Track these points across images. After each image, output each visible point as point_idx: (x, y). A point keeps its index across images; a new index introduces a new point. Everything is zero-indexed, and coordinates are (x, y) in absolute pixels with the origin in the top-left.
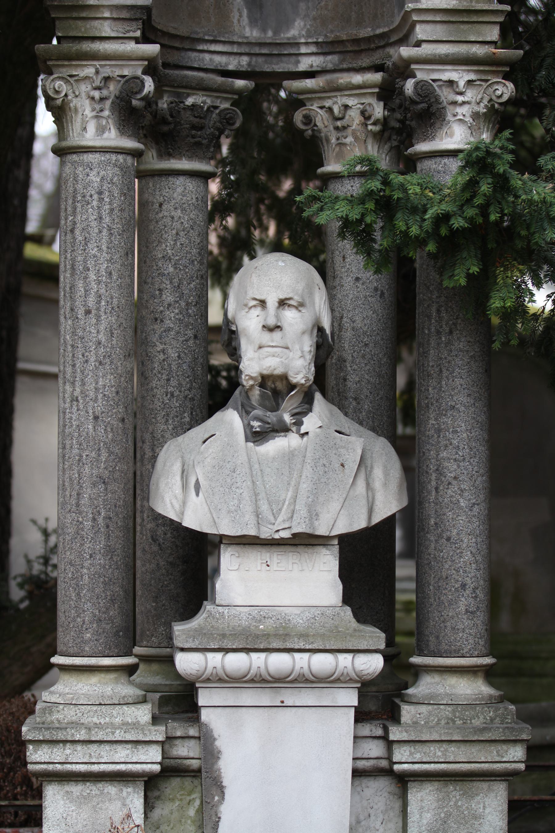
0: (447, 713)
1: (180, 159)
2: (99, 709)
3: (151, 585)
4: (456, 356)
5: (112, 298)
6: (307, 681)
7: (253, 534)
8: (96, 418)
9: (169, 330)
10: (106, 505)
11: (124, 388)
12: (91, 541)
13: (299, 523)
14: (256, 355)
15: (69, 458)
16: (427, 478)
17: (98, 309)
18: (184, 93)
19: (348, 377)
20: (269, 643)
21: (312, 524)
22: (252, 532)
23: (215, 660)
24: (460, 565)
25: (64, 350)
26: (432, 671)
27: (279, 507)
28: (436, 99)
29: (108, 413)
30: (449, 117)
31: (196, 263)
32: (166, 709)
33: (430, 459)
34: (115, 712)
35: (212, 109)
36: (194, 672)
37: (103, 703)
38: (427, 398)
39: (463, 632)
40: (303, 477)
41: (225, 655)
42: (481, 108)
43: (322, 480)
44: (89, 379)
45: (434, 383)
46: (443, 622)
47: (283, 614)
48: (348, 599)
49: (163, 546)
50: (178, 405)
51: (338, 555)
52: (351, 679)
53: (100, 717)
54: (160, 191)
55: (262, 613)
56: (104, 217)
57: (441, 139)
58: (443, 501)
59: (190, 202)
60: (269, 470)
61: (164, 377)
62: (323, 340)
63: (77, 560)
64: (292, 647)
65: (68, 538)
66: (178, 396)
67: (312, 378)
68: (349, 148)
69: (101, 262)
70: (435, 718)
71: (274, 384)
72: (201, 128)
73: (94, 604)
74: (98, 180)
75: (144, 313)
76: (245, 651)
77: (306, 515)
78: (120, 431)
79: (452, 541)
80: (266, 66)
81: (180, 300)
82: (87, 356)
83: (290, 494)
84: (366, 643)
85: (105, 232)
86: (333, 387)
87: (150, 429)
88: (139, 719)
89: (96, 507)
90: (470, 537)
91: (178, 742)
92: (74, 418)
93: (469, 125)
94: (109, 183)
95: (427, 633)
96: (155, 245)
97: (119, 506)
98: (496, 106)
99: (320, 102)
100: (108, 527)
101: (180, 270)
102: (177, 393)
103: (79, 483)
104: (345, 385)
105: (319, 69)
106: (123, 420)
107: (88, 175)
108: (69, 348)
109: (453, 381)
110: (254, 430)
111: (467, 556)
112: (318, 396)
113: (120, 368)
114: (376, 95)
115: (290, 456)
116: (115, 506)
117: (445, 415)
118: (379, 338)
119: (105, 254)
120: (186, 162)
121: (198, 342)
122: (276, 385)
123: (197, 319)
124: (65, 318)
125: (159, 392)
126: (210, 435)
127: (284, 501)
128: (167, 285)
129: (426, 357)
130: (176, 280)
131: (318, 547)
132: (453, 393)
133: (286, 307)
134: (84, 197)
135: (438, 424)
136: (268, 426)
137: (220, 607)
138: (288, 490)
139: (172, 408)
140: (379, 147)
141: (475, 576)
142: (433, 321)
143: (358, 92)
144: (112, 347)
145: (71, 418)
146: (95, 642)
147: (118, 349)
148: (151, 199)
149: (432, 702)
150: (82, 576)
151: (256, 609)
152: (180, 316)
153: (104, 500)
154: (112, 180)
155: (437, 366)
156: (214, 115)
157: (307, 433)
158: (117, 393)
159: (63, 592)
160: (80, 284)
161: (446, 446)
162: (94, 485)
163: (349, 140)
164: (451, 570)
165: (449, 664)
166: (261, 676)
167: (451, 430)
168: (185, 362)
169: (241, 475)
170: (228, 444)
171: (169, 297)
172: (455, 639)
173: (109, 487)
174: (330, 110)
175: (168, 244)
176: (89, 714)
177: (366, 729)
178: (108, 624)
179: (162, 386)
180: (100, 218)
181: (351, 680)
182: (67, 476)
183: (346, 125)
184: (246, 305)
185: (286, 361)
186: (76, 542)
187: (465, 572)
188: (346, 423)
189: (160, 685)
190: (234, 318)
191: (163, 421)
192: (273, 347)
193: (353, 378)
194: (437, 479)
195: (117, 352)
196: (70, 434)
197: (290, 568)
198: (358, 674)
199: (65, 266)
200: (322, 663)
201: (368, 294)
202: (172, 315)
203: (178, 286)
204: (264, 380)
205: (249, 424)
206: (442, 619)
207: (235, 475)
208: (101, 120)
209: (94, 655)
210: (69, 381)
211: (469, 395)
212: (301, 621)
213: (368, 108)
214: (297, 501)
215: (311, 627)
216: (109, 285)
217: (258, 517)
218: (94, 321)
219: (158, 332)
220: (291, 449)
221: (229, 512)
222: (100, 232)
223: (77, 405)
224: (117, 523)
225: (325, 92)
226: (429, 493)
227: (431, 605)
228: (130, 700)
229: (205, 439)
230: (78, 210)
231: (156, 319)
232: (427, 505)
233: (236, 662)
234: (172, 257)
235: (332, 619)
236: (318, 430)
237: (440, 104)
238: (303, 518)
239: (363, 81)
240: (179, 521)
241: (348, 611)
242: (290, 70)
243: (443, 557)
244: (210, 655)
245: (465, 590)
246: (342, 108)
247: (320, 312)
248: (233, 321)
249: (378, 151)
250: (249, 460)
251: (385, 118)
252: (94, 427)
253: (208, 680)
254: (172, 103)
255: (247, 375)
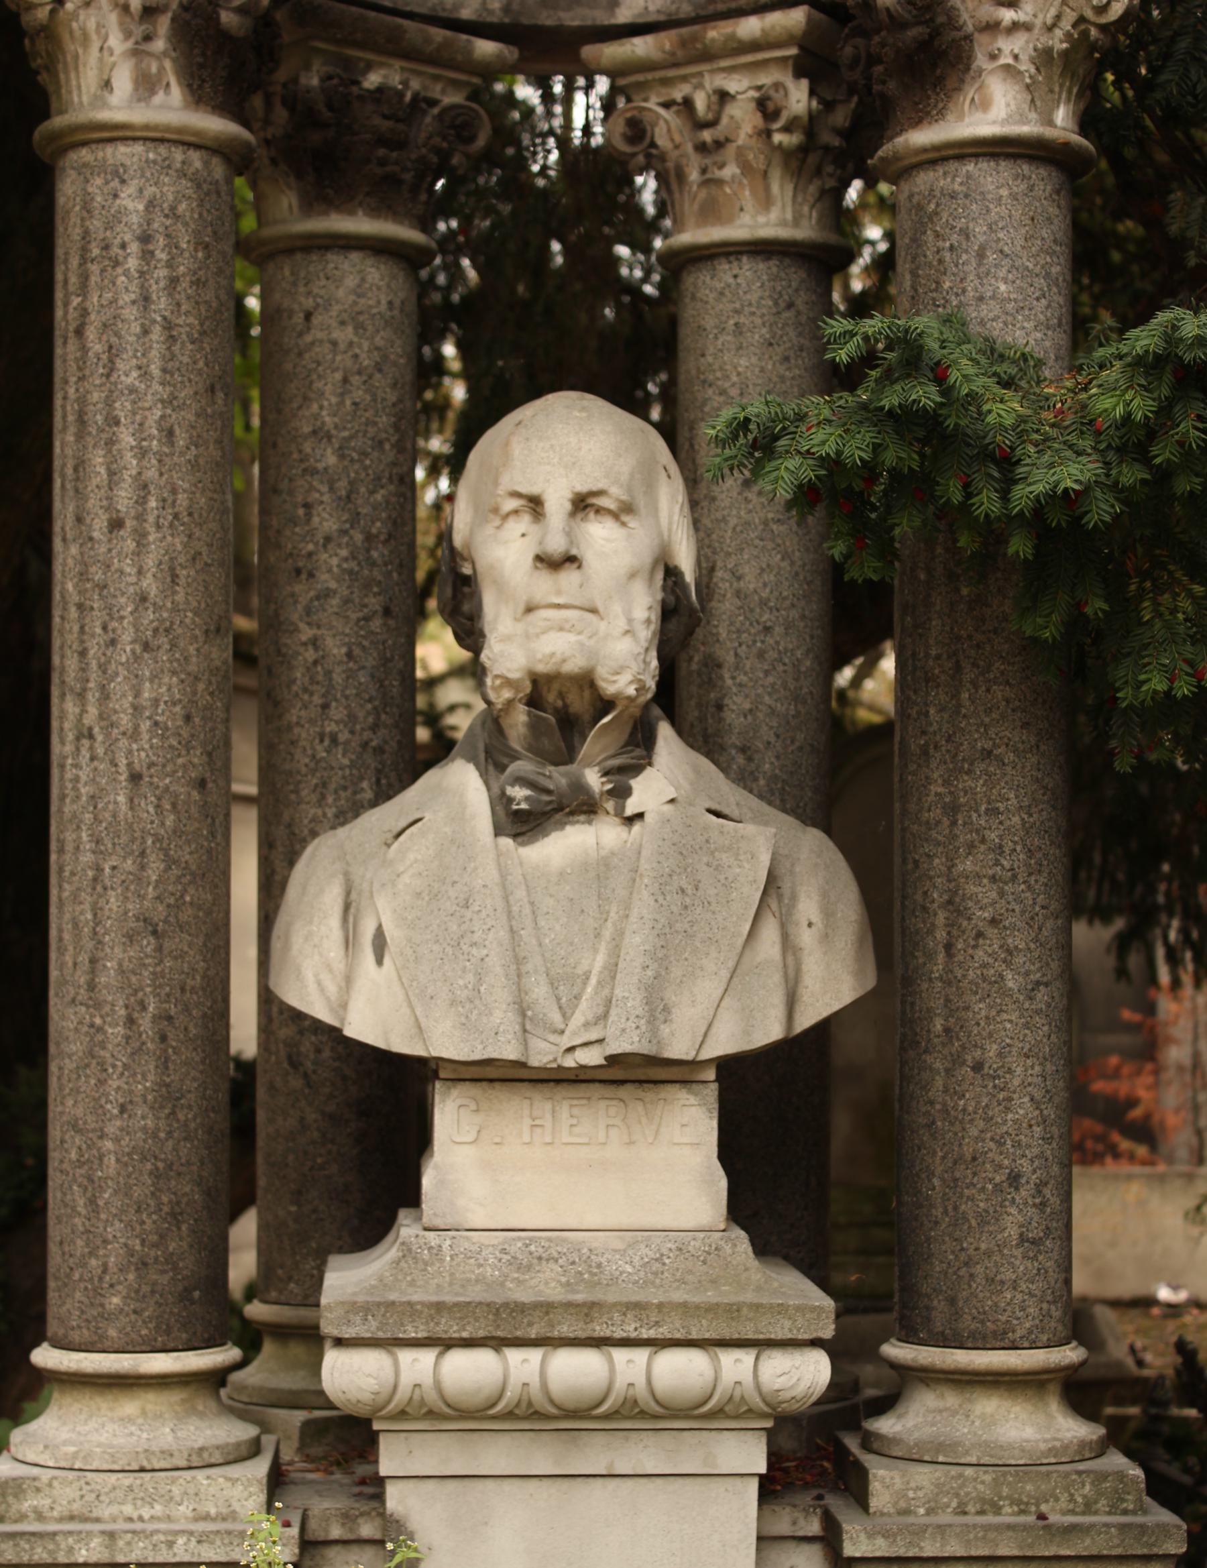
0: (981, 1487)
1: (351, 213)
2: (138, 1482)
3: (287, 1165)
4: (995, 631)
5: (174, 491)
6: (643, 1414)
7: (512, 1057)
8: (135, 778)
9: (327, 594)
10: (160, 986)
11: (205, 708)
12: (122, 1074)
13: (624, 1030)
14: (520, 628)
15: (73, 874)
16: (924, 922)
17: (140, 518)
18: (360, 59)
19: (726, 701)
20: (552, 1326)
21: (654, 1031)
22: (510, 1052)
23: (417, 1365)
24: (1005, 1128)
25: (63, 618)
26: (938, 1381)
27: (576, 991)
28: (950, 18)
29: (164, 766)
30: (981, 60)
31: (387, 446)
32: (317, 1450)
33: (931, 878)
34: (176, 1491)
35: (424, 105)
36: (366, 1397)
37: (148, 1467)
38: (924, 733)
39: (1015, 1288)
40: (634, 918)
41: (440, 1355)
42: (1057, 41)
43: (678, 926)
44: (118, 686)
45: (942, 697)
46: (966, 1264)
47: (585, 1251)
48: (740, 1210)
49: (314, 1077)
50: (346, 762)
51: (716, 1106)
52: (750, 1410)
53: (139, 1502)
54: (306, 285)
55: (532, 1248)
56: (154, 297)
57: (961, 118)
58: (964, 976)
59: (374, 311)
60: (551, 902)
61: (317, 700)
62: (678, 598)
63: (89, 1118)
64: (608, 1333)
65: (69, 1065)
66: (347, 742)
67: (652, 684)
68: (728, 190)
69: (147, 405)
70: (951, 1501)
71: (563, 699)
72: (400, 144)
73: (129, 1225)
74: (141, 207)
75: (272, 559)
76: (493, 1343)
77: (639, 1011)
78: (194, 810)
79: (986, 1070)
80: (545, 14)
81: (352, 527)
82: (114, 630)
83: (600, 960)
84: (787, 1324)
85: (157, 334)
86: (692, 726)
87: (286, 817)
88: (236, 1506)
89: (136, 991)
90: (1029, 1062)
91: (332, 1552)
92: (84, 778)
93: (1028, 81)
94: (166, 216)
95: (925, 1289)
96: (295, 405)
97: (193, 988)
98: (1094, 32)
99: (664, 91)
100: (163, 1038)
101: (352, 460)
102: (344, 736)
103: (95, 933)
104: (721, 720)
105: (662, 18)
106: (202, 784)
107: (116, 196)
108: (73, 613)
109: (988, 690)
110: (515, 807)
111: (1023, 1109)
112: (665, 732)
113: (194, 659)
114: (790, 62)
115: (600, 870)
116: (183, 990)
117: (968, 772)
118: (794, 614)
119: (156, 387)
120: (365, 219)
121: (392, 622)
122: (568, 701)
123: (390, 573)
124: (64, 540)
125: (304, 734)
126: (411, 819)
127: (587, 976)
128: (322, 494)
129: (921, 635)
130: (342, 486)
131: (669, 1087)
132: (987, 720)
133: (592, 515)
134: (106, 247)
135: (951, 793)
136: (546, 798)
137: (432, 1234)
138: (596, 951)
139: (332, 768)
140: (795, 188)
141: (1041, 1156)
142: (939, 550)
143: (749, 58)
144: (175, 609)
145: (77, 779)
146: (133, 1317)
147: (189, 614)
148: (286, 303)
149: (941, 1459)
150: (101, 1158)
151: (519, 1239)
152: (352, 565)
153: (154, 973)
154: (173, 209)
155: (949, 657)
156: (428, 120)
157: (640, 816)
158: (188, 718)
159: (59, 1195)
160: (98, 459)
161: (971, 846)
162: (130, 938)
163: (730, 171)
164: (983, 1140)
165: (983, 1367)
166: (530, 1404)
167: (983, 808)
168: (363, 668)
169: (483, 914)
170: (453, 841)
171: (327, 521)
172: (996, 1305)
173: (168, 945)
174: (688, 103)
175: (326, 403)
176: (112, 1495)
177: (783, 1523)
178: (163, 1272)
179: (312, 721)
180: (145, 299)
181: (751, 1413)
182: (67, 916)
183: (722, 139)
184: (495, 510)
185: (592, 642)
186: (87, 1076)
187: (1017, 1144)
188: (731, 795)
189: (306, 1391)
190: (468, 545)
191: (314, 798)
192: (558, 606)
193: (737, 704)
194: (950, 924)
195: (187, 621)
196: (74, 816)
197: (601, 1136)
198: (768, 1399)
199: (64, 417)
200: (681, 1371)
201: (770, 515)
202: (335, 561)
203: (348, 497)
204: (539, 690)
205: (503, 793)
206: (963, 1256)
207: (468, 914)
208: (146, 60)
209: (130, 1348)
210: (72, 690)
211: (1025, 725)
212: (629, 1269)
213: (772, 93)
214: (619, 976)
215: (653, 1283)
216: (167, 460)
217: (524, 1015)
218: (130, 545)
219: (303, 600)
220: (603, 853)
221: (453, 1003)
222: (146, 332)
223: (91, 748)
224: (186, 1029)
225: (676, 65)
226: (930, 956)
227: (936, 1223)
228: (217, 1457)
229: (399, 828)
230: (94, 279)
231: (298, 572)
232: (925, 986)
233: (471, 1371)
234: (334, 432)
235: (704, 1262)
236: (669, 808)
237: (959, 29)
238: (632, 1018)
239: (763, 30)
240: (336, 1023)
241: (740, 1243)
242: (598, 22)
243: (964, 1110)
244: (406, 1356)
245: (1017, 1189)
246: (714, 98)
247: (670, 530)
248: (465, 554)
249: (794, 196)
250: (503, 876)
251: (812, 117)
252: (131, 800)
253: (402, 1415)
254: (330, 78)
255: (497, 676)
